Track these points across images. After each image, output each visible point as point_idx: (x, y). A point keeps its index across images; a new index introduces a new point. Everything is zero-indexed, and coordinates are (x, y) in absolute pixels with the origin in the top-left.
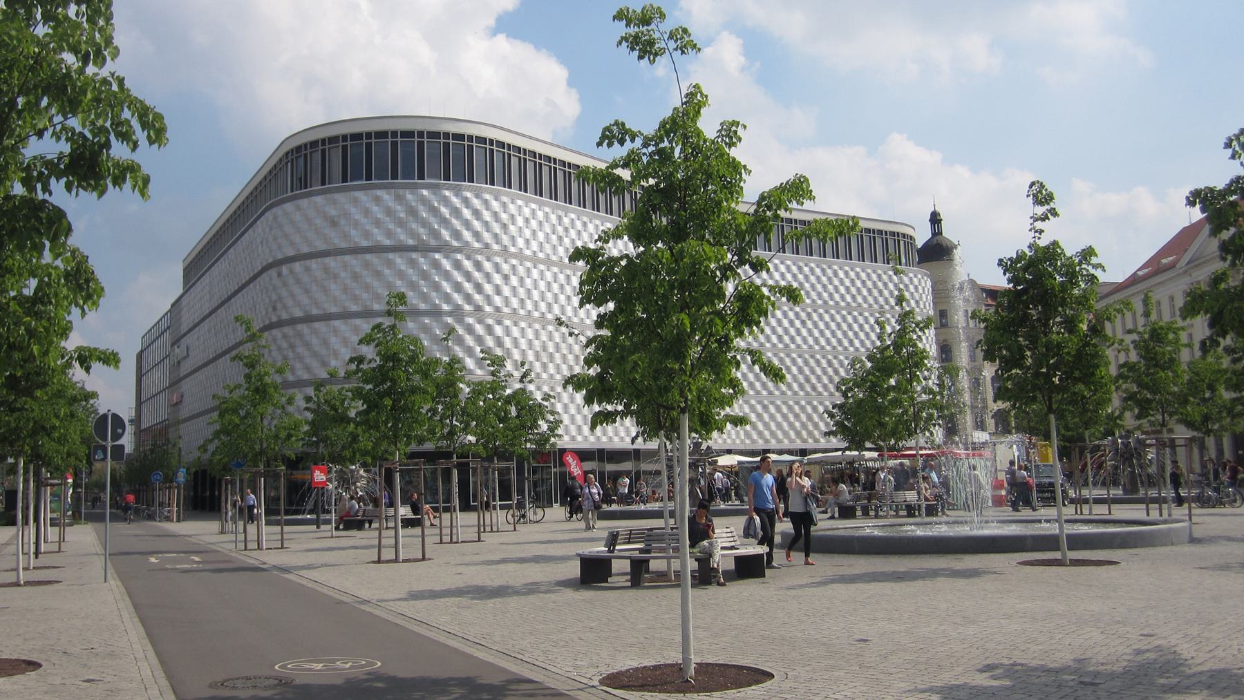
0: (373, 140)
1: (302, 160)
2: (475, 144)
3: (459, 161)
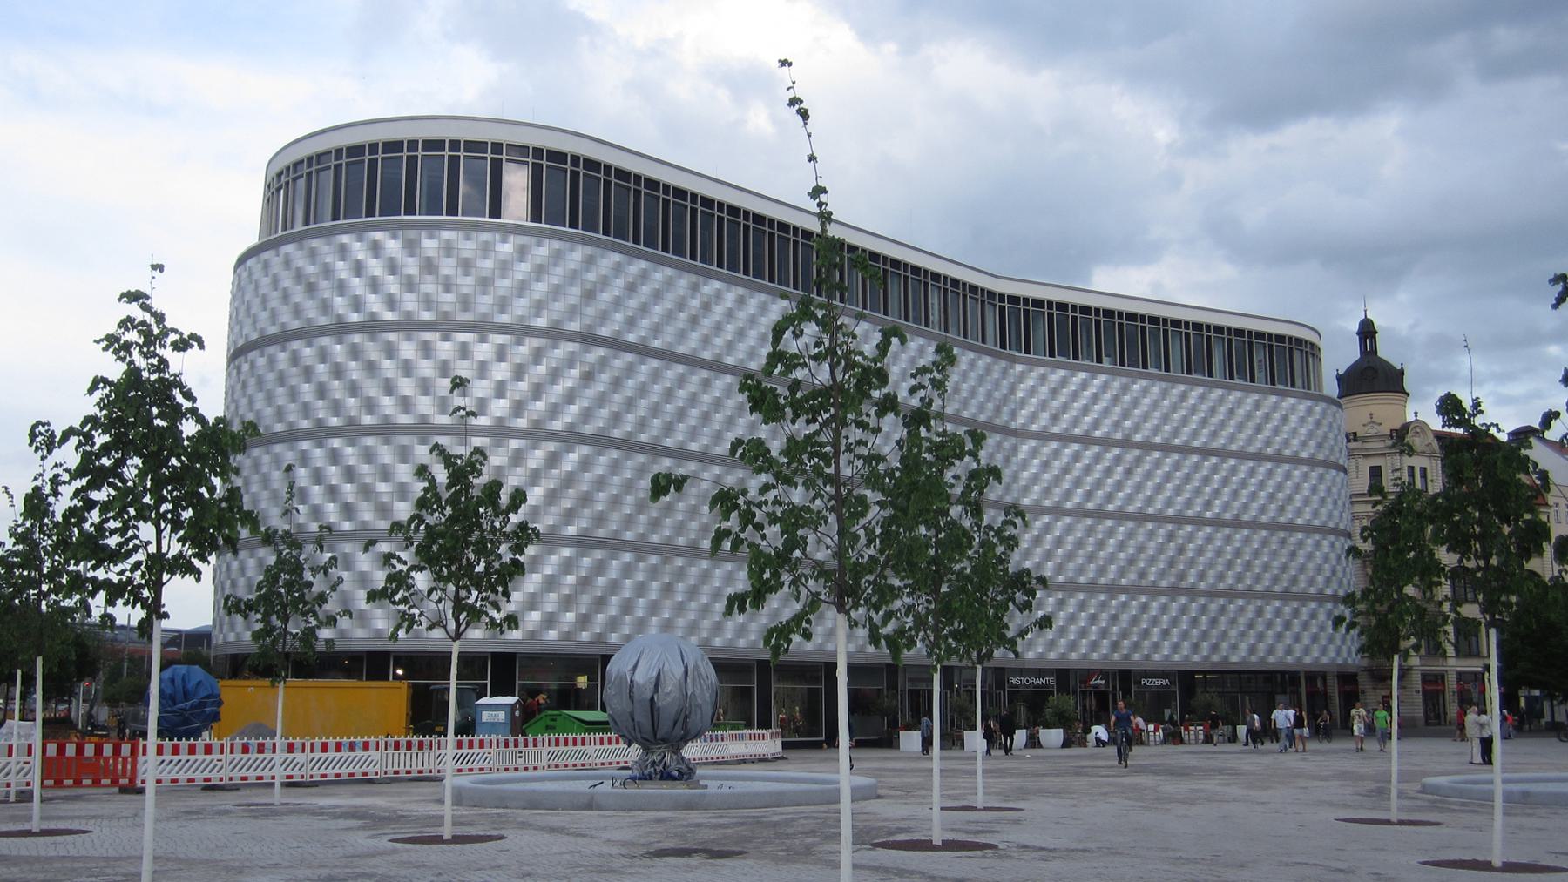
0: (380, 156)
1: (302, 183)
2: (545, 163)
3: (758, 258)
